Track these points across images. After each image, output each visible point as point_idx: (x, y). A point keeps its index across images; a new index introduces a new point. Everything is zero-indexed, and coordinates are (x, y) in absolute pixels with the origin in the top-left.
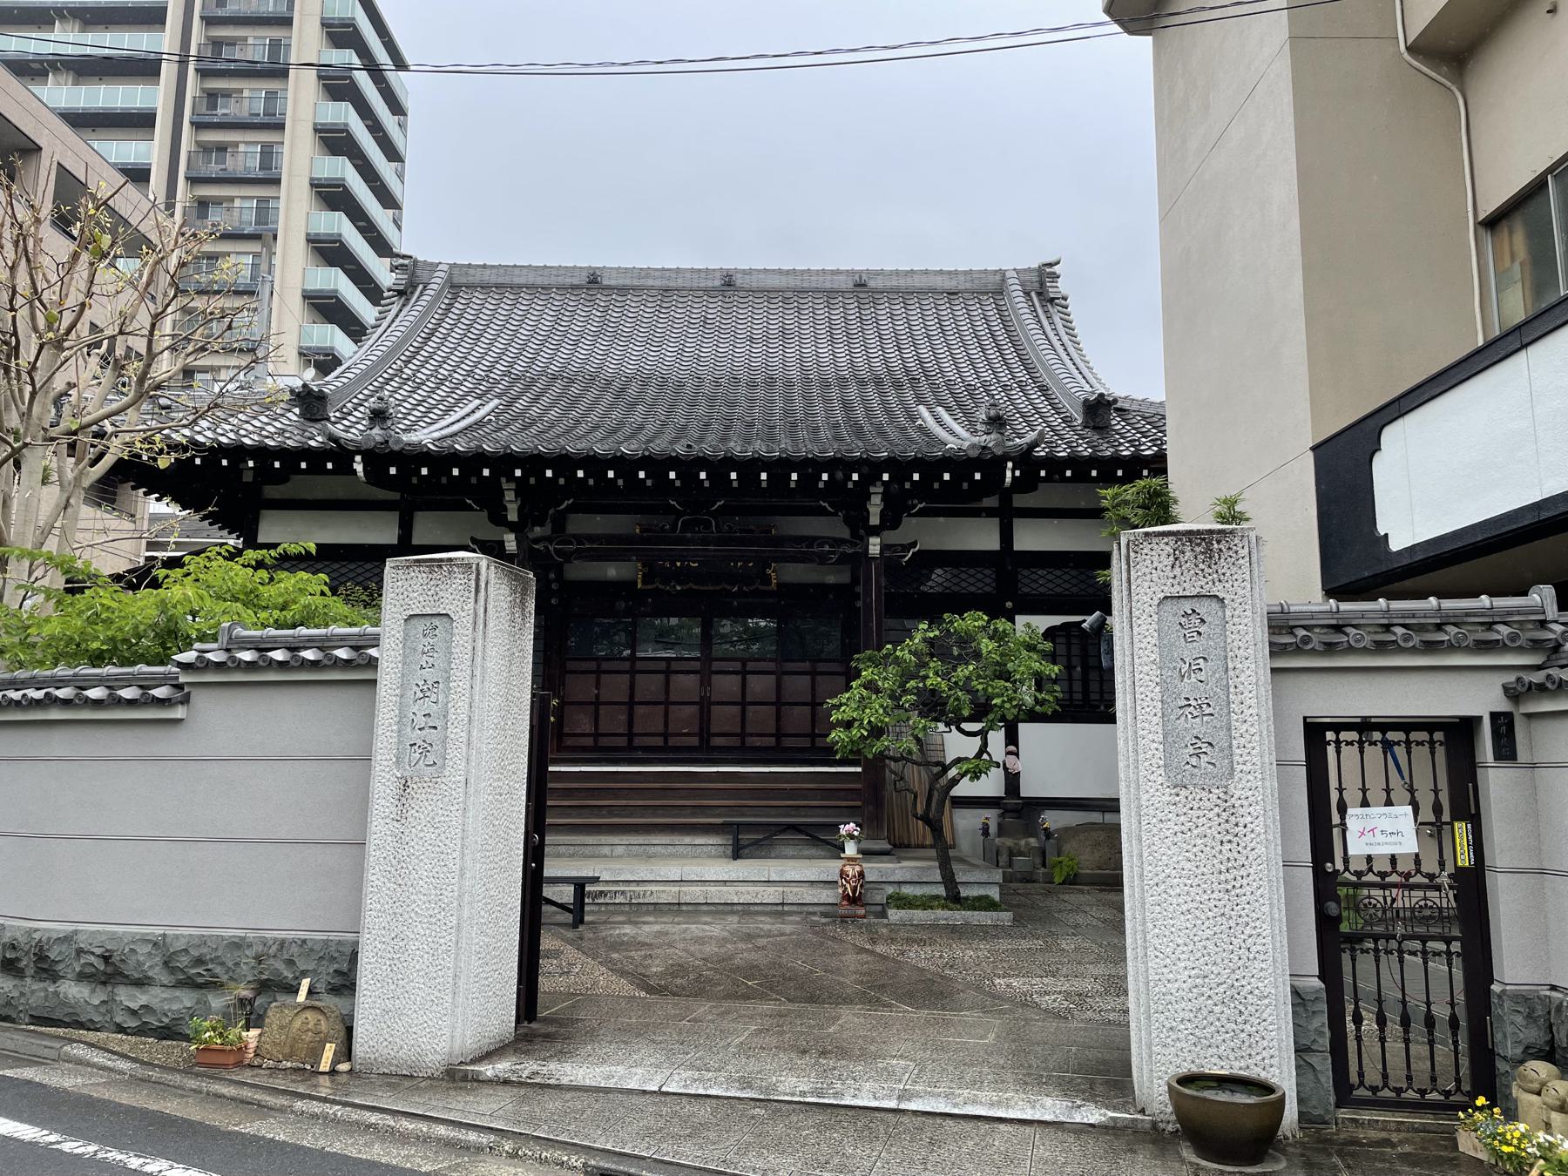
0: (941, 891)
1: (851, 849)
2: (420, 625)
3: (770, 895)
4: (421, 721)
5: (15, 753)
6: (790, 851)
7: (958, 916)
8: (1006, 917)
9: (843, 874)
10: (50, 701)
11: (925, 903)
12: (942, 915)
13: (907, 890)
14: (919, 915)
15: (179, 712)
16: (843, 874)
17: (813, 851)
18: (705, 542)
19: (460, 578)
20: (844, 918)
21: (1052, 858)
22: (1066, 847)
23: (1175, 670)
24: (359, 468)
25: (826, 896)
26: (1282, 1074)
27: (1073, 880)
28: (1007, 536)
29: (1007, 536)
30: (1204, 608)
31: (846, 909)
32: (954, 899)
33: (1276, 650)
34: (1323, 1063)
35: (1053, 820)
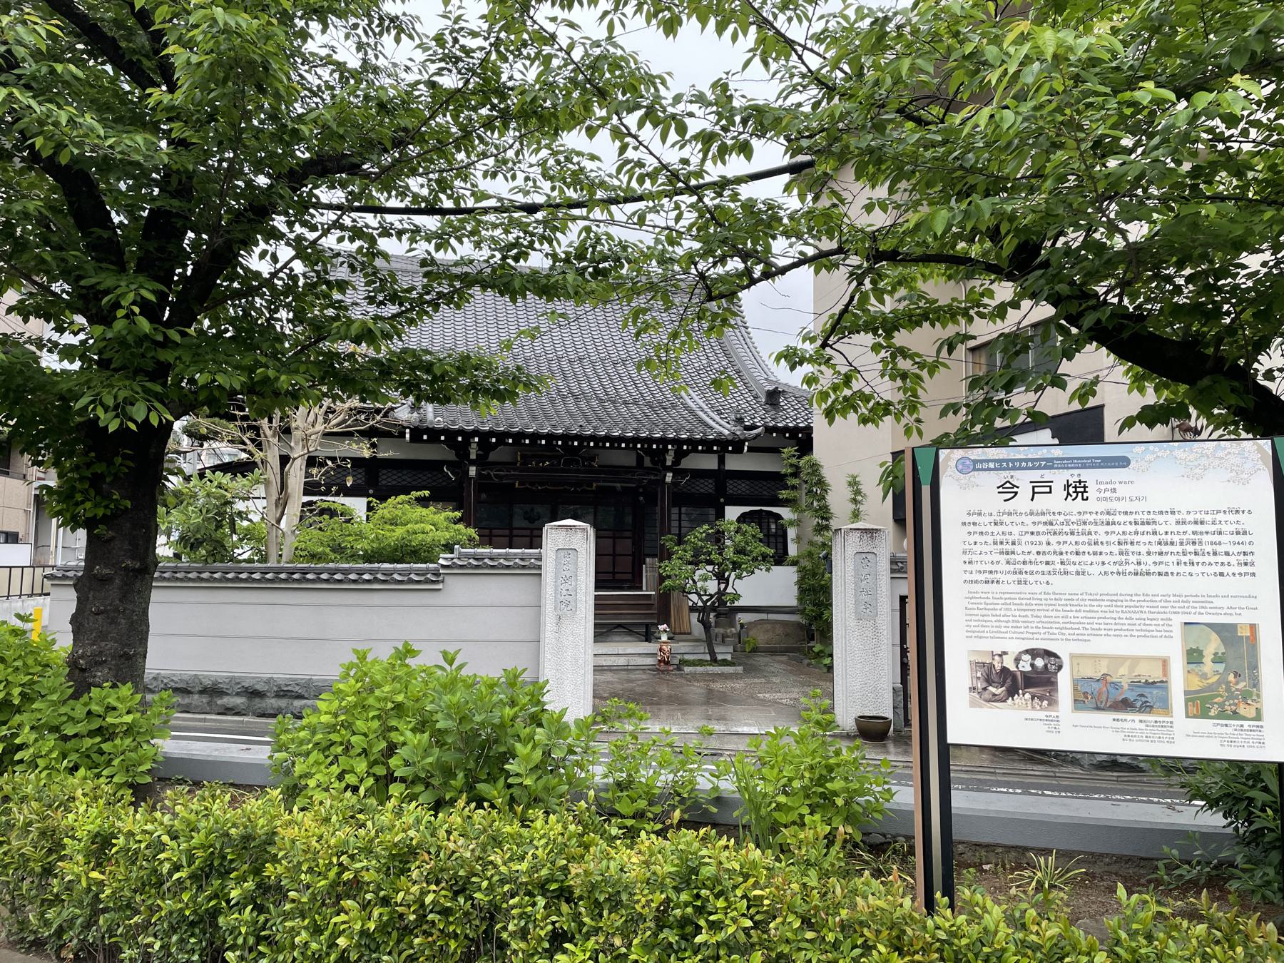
0: (708, 657)
1: (664, 638)
2: (562, 553)
3: (622, 661)
4: (564, 592)
5: (300, 602)
6: (617, 638)
7: (717, 669)
8: (740, 669)
9: (661, 650)
10: (376, 580)
11: (701, 663)
12: (711, 669)
13: (687, 657)
14: (699, 669)
15: (440, 586)
16: (661, 650)
17: (629, 638)
18: (578, 471)
19: (580, 534)
20: (663, 672)
21: (744, 638)
22: (751, 633)
23: (858, 578)
24: (408, 436)
25: (649, 661)
26: (889, 714)
27: (755, 650)
28: (722, 461)
29: (722, 461)
30: (869, 556)
31: (663, 667)
32: (714, 661)
33: (893, 571)
34: (901, 712)
35: (743, 618)
